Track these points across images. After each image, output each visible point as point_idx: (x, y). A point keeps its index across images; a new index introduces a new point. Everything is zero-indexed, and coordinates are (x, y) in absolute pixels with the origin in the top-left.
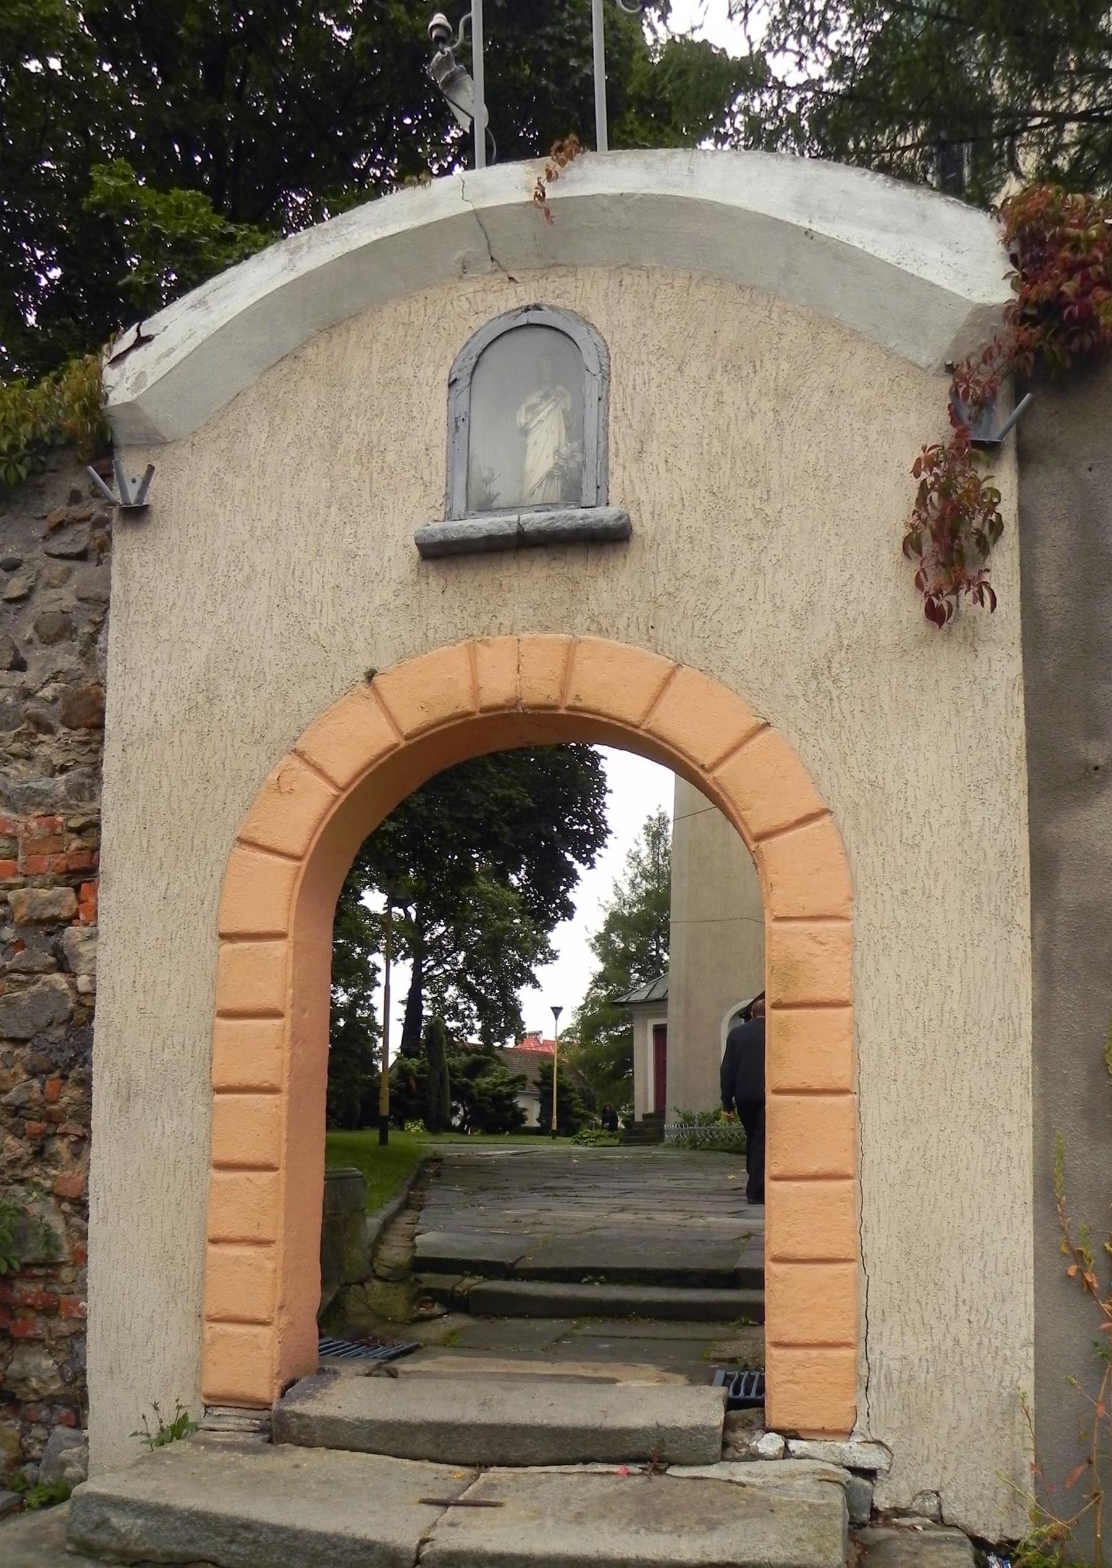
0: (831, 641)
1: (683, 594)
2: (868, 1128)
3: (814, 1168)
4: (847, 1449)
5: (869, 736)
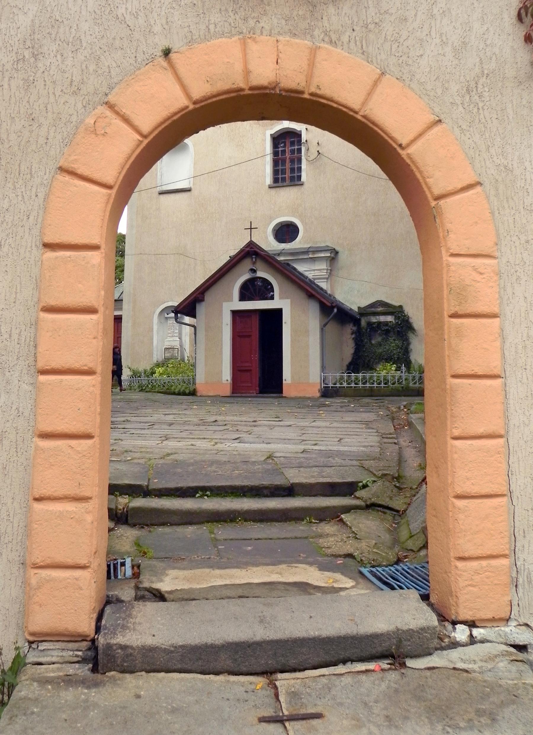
0: (477, 70)
1: (384, 25)
2: (511, 402)
3: (481, 430)
4: (509, 632)
5: (502, 136)
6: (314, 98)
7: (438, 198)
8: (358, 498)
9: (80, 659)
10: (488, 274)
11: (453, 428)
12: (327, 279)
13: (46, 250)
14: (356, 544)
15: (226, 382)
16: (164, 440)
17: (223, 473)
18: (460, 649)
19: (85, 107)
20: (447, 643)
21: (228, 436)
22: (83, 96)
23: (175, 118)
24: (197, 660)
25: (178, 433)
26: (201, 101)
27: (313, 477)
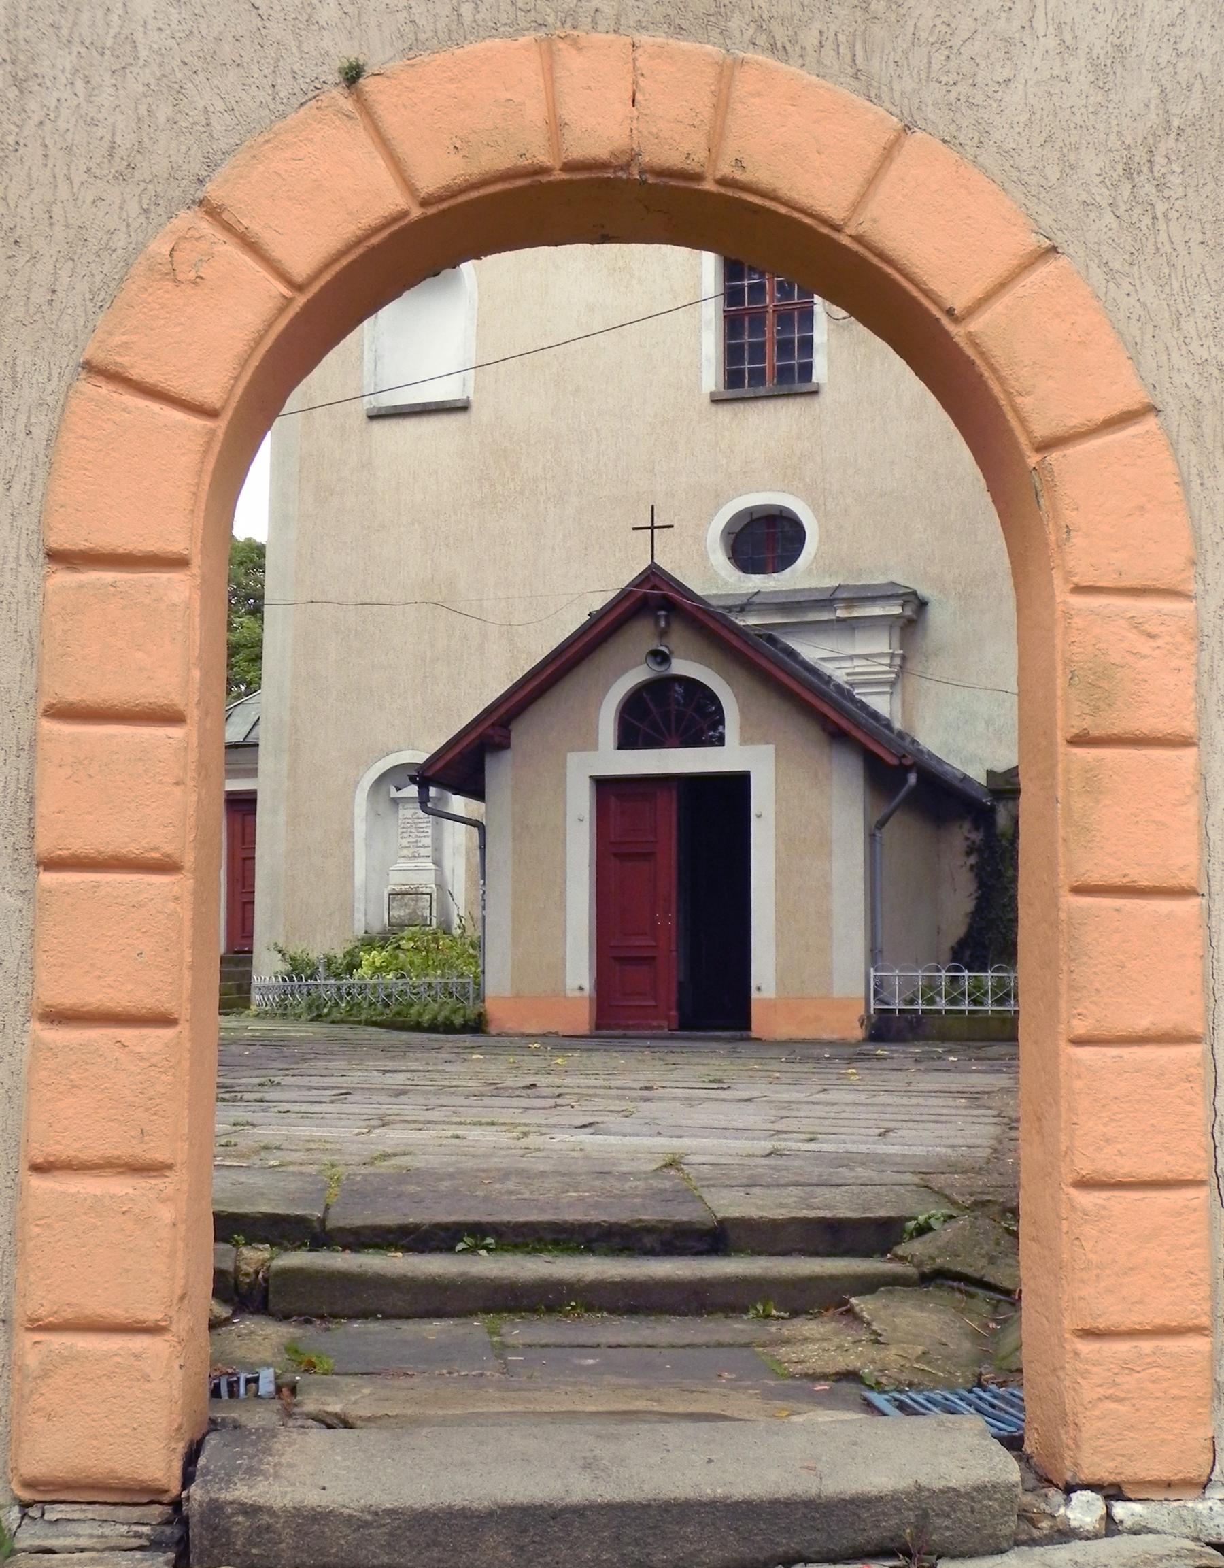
0: (1153, 118)
3: (1142, 1023)
4: (1205, 1512)
6: (730, 192)
7: (1045, 446)
8: (902, 1259)
9: (147, 1543)
10: (1168, 639)
11: (1074, 1016)
12: (892, 684)
13: (54, 567)
14: (873, 1352)
15: (578, 994)
16: (375, 1127)
17: (534, 1197)
18: (1077, 1545)
19: (146, 211)
20: (1046, 1532)
21: (564, 1120)
22: (143, 185)
23: (374, 241)
24: (428, 1545)
25: (416, 1113)
26: (441, 199)
27: (781, 1205)
